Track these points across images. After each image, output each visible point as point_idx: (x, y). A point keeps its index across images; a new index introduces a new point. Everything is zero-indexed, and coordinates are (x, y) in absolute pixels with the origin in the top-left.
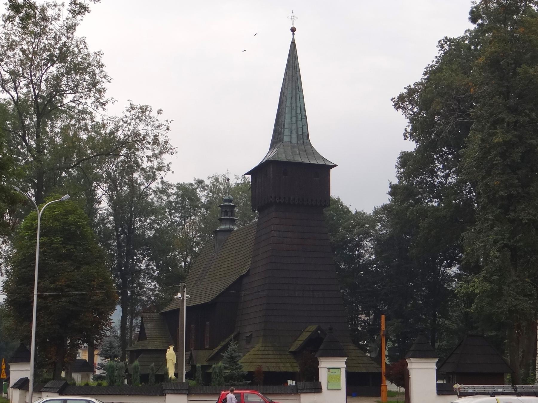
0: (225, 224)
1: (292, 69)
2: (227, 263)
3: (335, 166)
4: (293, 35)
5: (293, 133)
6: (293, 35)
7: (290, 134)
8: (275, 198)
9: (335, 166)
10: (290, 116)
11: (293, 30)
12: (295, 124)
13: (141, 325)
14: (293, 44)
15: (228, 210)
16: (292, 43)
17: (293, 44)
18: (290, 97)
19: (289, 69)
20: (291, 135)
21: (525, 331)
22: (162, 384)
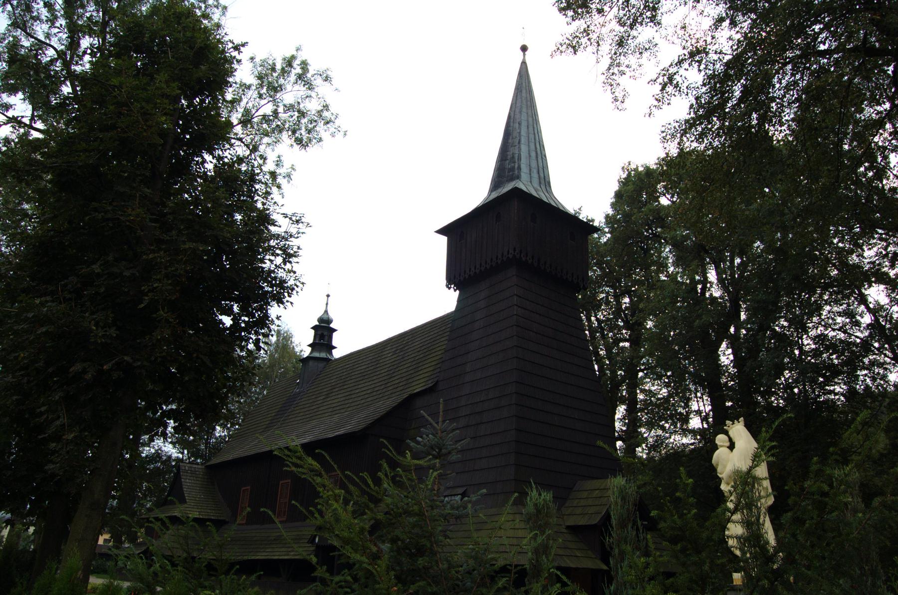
0: (320, 351)
1: (526, 92)
2: (325, 390)
3: (336, 348)
4: (524, 55)
5: (533, 172)
6: (524, 55)
7: (528, 172)
8: (521, 252)
9: (336, 348)
10: (527, 149)
11: (524, 49)
12: (536, 161)
13: (733, 353)
14: (524, 63)
15: (326, 333)
16: (522, 63)
17: (524, 63)
18: (526, 124)
19: (521, 91)
20: (530, 174)
21: (386, 485)
22: (346, 541)
